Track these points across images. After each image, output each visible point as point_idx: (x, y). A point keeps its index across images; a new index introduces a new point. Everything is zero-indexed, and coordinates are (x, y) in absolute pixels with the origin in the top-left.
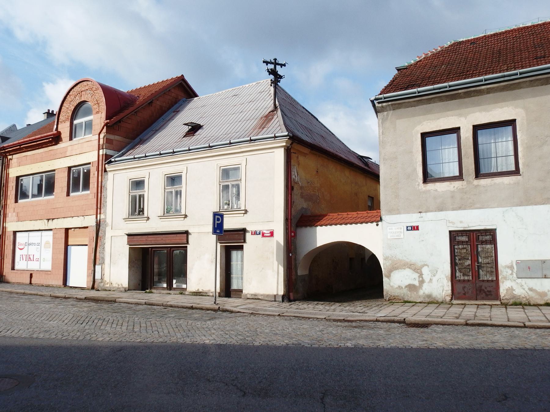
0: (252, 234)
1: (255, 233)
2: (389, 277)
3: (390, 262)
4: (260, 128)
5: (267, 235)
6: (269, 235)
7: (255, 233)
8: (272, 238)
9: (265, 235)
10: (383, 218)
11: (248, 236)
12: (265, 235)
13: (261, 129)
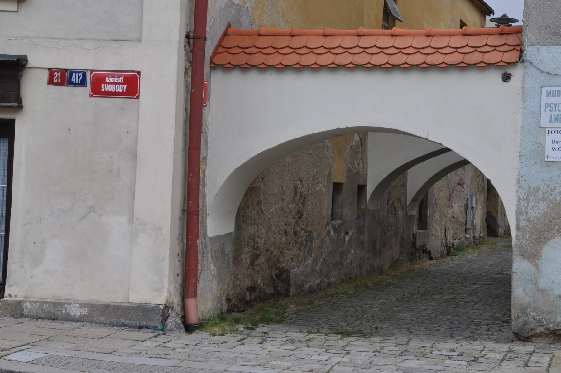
0: (51, 82)
1: (62, 78)
2: (533, 257)
3: (543, 206)
4: (238, 341)
5: (113, 88)
6: (121, 88)
7: (62, 78)
8: (130, 102)
9: (104, 88)
10: (530, 52)
11: (35, 89)
12: (104, 88)
13: (239, 343)
